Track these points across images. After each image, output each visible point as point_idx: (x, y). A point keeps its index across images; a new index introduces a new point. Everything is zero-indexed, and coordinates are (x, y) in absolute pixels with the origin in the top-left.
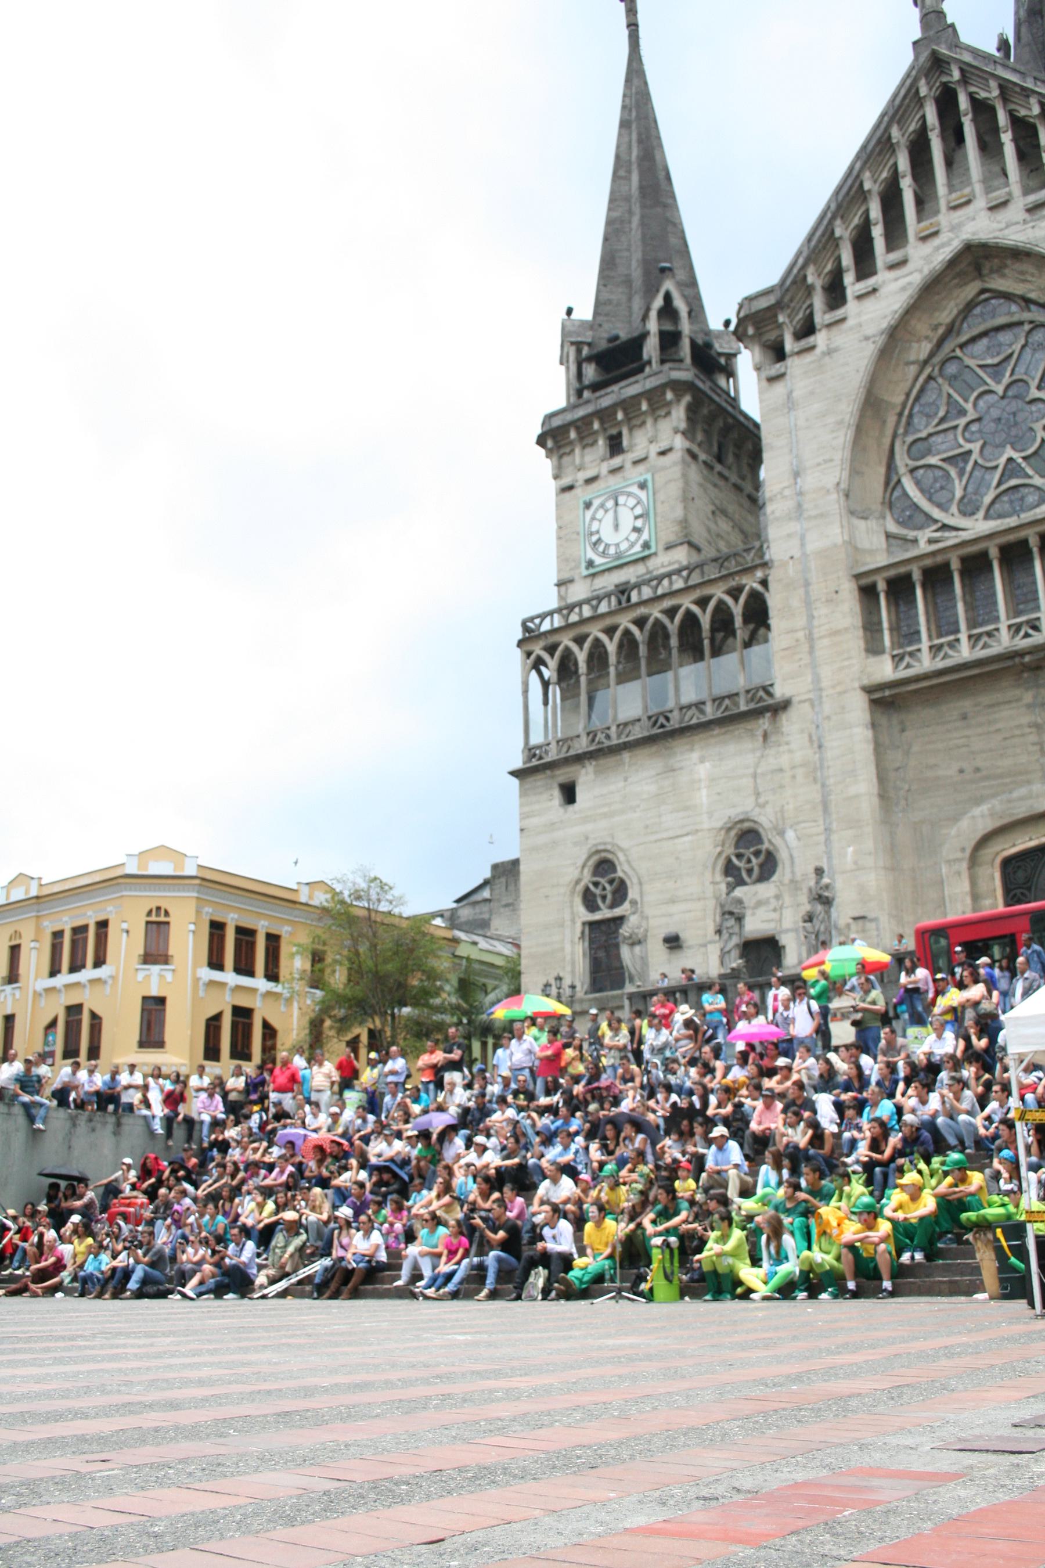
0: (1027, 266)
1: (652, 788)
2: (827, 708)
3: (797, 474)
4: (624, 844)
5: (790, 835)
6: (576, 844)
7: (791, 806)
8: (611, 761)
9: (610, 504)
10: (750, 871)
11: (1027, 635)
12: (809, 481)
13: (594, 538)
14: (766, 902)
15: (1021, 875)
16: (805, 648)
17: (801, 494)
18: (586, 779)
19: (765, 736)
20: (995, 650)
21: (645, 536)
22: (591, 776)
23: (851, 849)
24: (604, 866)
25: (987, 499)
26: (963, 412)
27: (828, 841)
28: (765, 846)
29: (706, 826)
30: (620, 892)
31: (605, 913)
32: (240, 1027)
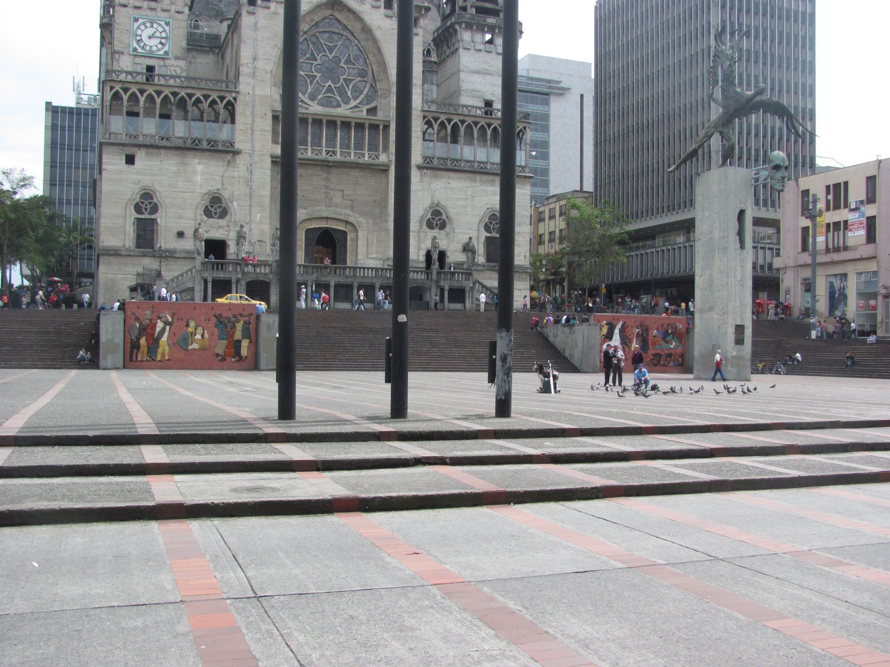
0: (351, 16)
1: (175, 169)
2: (256, 159)
3: (255, 59)
4: (159, 189)
5: (235, 203)
6: (133, 183)
8: (155, 151)
9: (164, 35)
10: (216, 213)
12: (260, 64)
13: (138, 38)
14: (223, 227)
16: (250, 132)
17: (255, 68)
18: (141, 157)
19: (229, 162)
20: (319, 157)
21: (166, 48)
22: (144, 155)
24: (147, 196)
25: (319, 97)
26: (316, 60)
27: (250, 210)
28: (224, 205)
29: (198, 191)
31: (146, 216)
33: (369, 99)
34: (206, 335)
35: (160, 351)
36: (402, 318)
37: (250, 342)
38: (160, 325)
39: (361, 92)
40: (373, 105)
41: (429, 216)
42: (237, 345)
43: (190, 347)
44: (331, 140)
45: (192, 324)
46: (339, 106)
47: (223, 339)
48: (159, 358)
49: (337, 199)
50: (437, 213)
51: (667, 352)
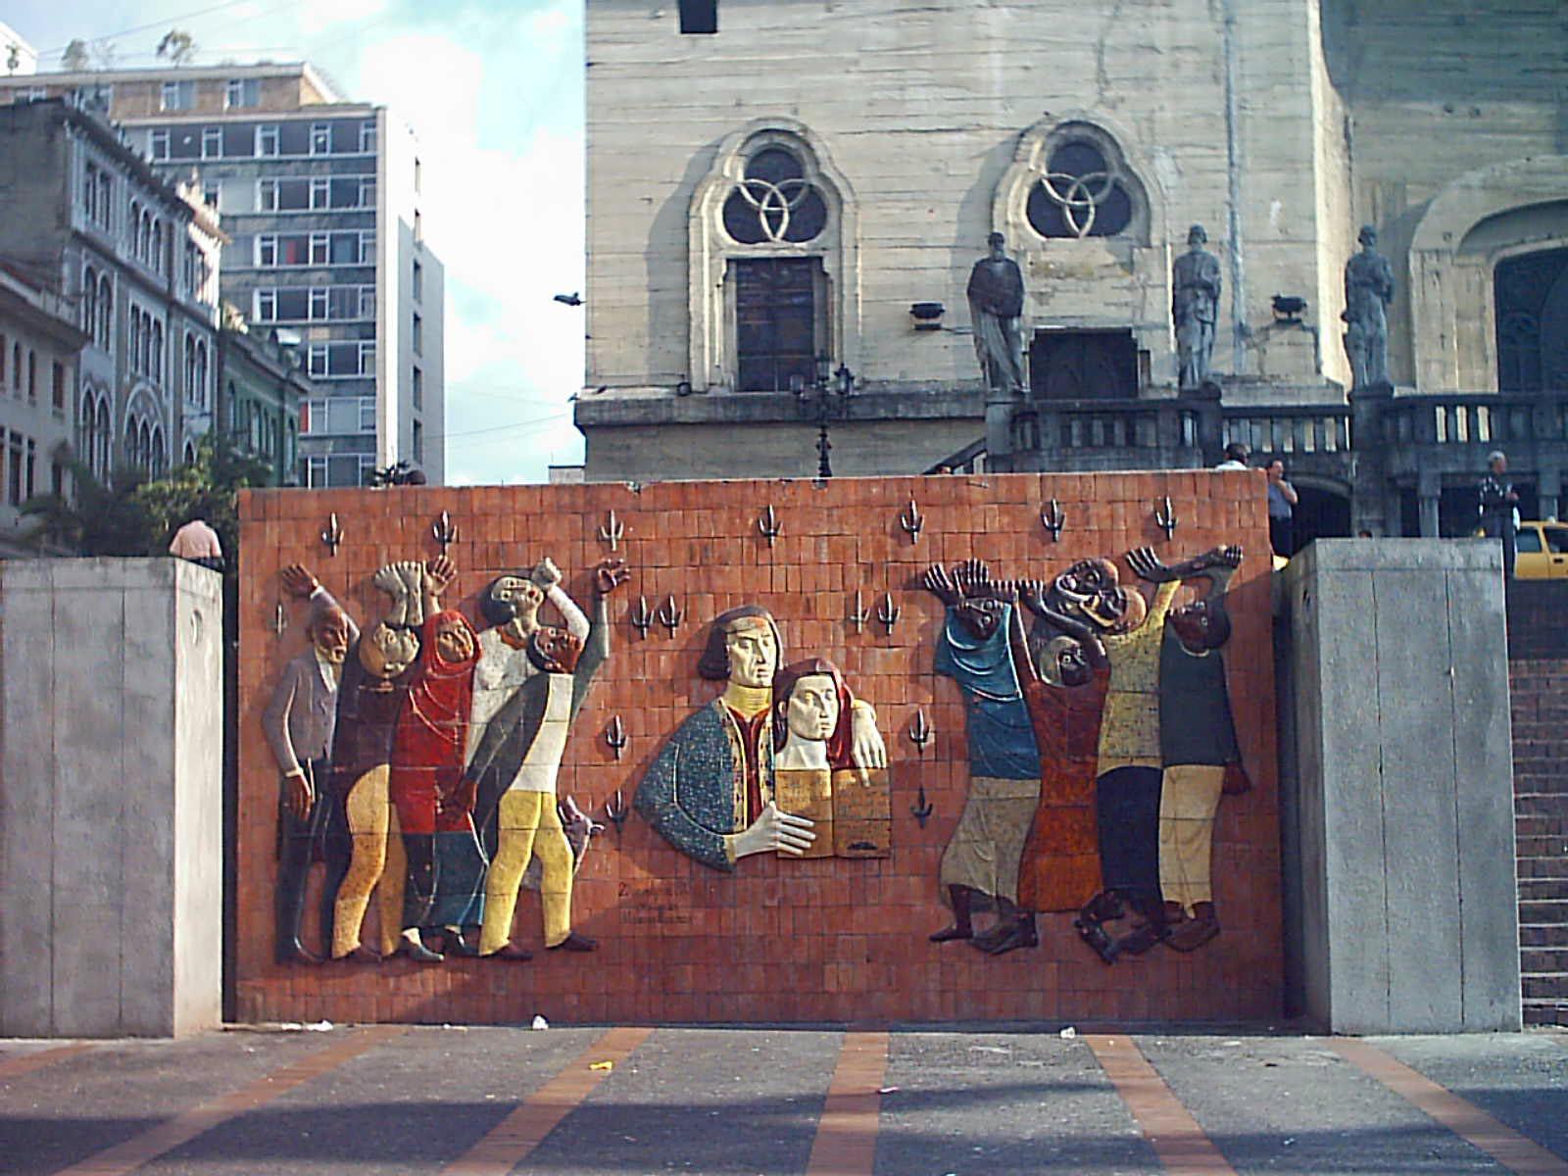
5: (1164, 164)
7: (1168, 115)
10: (1080, 215)
23: (1276, 205)
24: (779, 159)
30: (813, 212)
31: (777, 246)
32: (347, 311)
34: (868, 735)
35: (508, 879)
37: (1234, 788)
38: (497, 669)
42: (1127, 808)
43: (739, 843)
45: (758, 651)
47: (1004, 769)
48: (500, 929)
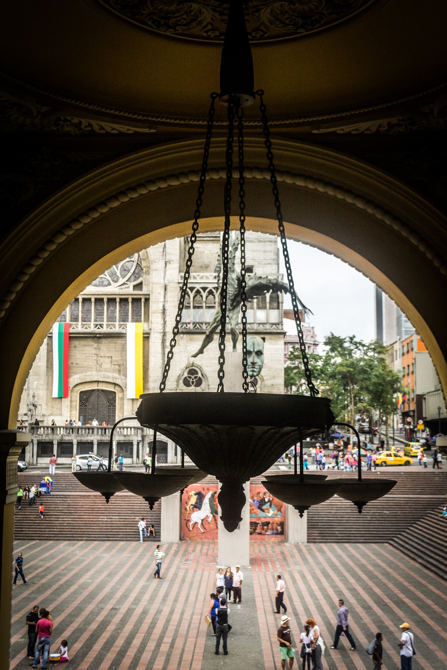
11: (99, 328)
15: (85, 397)
20: (89, 330)
33: (136, 275)
36: (381, 400)
39: (129, 271)
40: (138, 281)
41: (186, 375)
44: (99, 314)
46: (109, 284)
49: (106, 363)
50: (192, 372)
51: (263, 520)
